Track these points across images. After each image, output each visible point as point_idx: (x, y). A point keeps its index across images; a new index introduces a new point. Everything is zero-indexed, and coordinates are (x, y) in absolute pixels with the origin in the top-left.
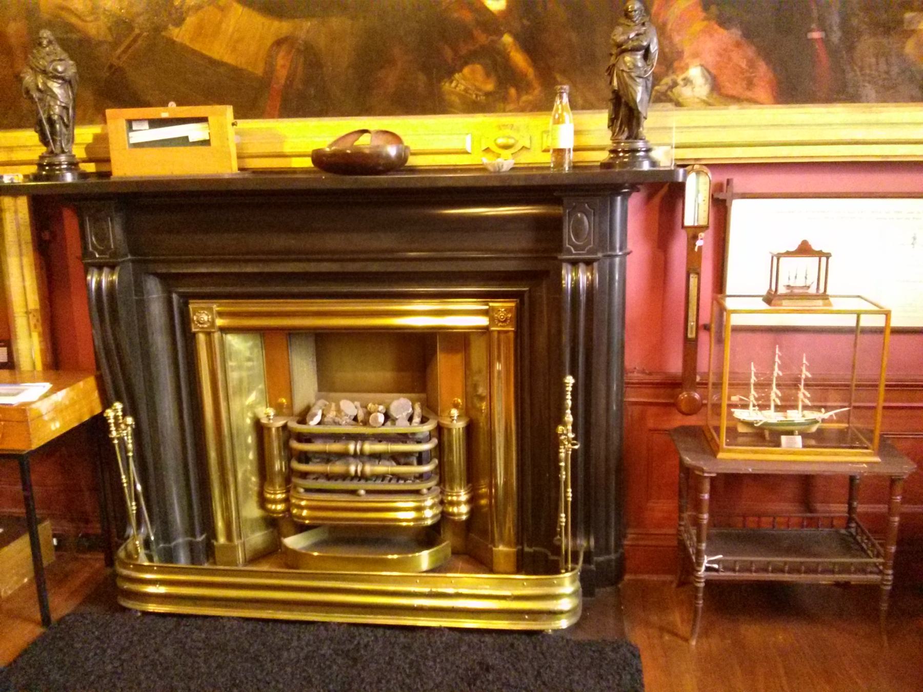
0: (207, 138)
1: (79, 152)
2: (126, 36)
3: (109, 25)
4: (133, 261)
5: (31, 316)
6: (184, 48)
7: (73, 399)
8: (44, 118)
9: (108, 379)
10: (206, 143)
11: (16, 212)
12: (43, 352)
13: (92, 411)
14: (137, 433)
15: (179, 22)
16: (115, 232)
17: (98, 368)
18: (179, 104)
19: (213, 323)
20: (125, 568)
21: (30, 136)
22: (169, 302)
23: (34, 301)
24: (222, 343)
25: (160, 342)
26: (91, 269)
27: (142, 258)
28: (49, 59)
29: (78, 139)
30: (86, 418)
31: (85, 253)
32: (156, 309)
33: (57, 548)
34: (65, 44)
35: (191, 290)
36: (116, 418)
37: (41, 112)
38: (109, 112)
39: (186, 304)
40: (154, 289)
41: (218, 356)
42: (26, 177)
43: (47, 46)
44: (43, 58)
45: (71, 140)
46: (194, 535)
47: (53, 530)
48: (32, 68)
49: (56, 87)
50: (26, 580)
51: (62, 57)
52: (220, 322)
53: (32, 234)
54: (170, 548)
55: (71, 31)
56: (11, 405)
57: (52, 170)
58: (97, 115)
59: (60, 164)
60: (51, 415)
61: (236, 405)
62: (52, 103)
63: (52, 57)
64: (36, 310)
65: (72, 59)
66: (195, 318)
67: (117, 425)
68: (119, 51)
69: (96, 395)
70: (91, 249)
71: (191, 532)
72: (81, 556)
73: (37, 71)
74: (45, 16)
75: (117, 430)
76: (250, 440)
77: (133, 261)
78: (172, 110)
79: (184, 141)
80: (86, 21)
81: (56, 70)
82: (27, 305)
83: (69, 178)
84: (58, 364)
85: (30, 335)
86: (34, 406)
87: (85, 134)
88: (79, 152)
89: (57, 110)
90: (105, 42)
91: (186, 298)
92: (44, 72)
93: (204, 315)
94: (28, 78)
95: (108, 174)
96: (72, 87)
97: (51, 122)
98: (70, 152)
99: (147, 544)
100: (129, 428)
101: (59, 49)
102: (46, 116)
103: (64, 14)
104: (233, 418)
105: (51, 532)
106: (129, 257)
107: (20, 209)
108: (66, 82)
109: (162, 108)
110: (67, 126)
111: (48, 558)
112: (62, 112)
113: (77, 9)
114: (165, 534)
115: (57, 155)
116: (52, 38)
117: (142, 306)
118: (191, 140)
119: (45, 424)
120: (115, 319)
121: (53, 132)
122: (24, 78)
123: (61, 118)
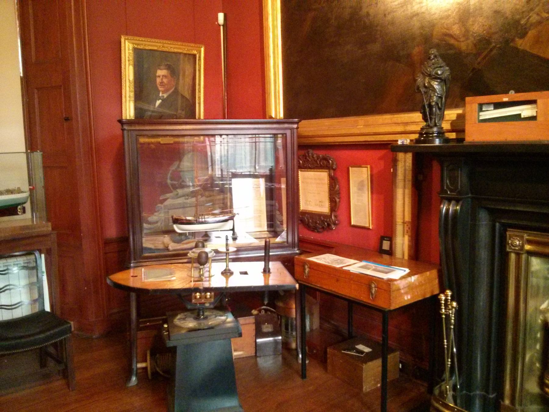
0: (535, 115)
1: (446, 126)
2: (485, 49)
3: (475, 42)
4: (472, 198)
5: (405, 225)
6: (524, 52)
7: (421, 282)
8: (426, 103)
9: (445, 272)
10: (533, 118)
11: (405, 161)
12: (410, 247)
13: (432, 291)
14: (459, 313)
15: (523, 35)
16: (462, 178)
17: (440, 265)
18: (517, 91)
19: (522, 247)
20: (437, 403)
21: (417, 116)
22: (493, 227)
23: (408, 218)
24: (528, 264)
25: (483, 254)
26: (444, 201)
27: (478, 197)
28: (433, 67)
29: (447, 117)
30: (428, 295)
31: (443, 191)
32: (483, 232)
33: (401, 370)
34: (444, 57)
35: (510, 222)
36: (446, 300)
37: (425, 101)
38: (468, 99)
39: (506, 231)
40: (484, 218)
41: (524, 273)
42: (411, 141)
43: (433, 59)
44: (430, 67)
45: (442, 117)
46: (487, 392)
47: (401, 358)
48: (423, 73)
49: (436, 85)
50: (379, 385)
51: (442, 65)
52: (527, 247)
53: (412, 177)
54: (469, 396)
55: (451, 49)
56: (383, 279)
57: (427, 137)
58: (459, 102)
59: (433, 133)
60: (406, 290)
61: (531, 304)
62: (432, 95)
63: (436, 66)
64: (409, 222)
65: (448, 66)
66: (510, 242)
67: (446, 305)
68: (479, 59)
69: (437, 281)
70: (445, 188)
71: (486, 388)
72: (414, 380)
73: (425, 75)
74: (436, 41)
75: (445, 309)
76: (539, 335)
77: (472, 198)
78: (512, 95)
79: (517, 117)
80: (460, 42)
81: (437, 74)
82: (37, 272)
83: (437, 142)
84: (417, 259)
85: (404, 236)
86: (395, 283)
87: (451, 114)
88: (446, 126)
89: (435, 99)
90: (472, 53)
91: (505, 227)
92: (430, 75)
93: (516, 241)
94: (419, 80)
95: (463, 140)
96: (446, 84)
97: (430, 106)
98: (440, 125)
99: (454, 388)
100: (454, 310)
101: (441, 60)
102: (427, 103)
103: (447, 38)
104: (528, 317)
105: (398, 360)
106: (470, 195)
107: (408, 160)
108: (443, 81)
109: (504, 95)
110: (440, 109)
111: (392, 376)
112: (437, 100)
113: (455, 34)
114: (468, 384)
115: (431, 127)
116: (437, 53)
117: (474, 230)
118: (522, 117)
119: (401, 295)
120: (454, 235)
121: (431, 113)
122: (417, 80)
123: (437, 104)
